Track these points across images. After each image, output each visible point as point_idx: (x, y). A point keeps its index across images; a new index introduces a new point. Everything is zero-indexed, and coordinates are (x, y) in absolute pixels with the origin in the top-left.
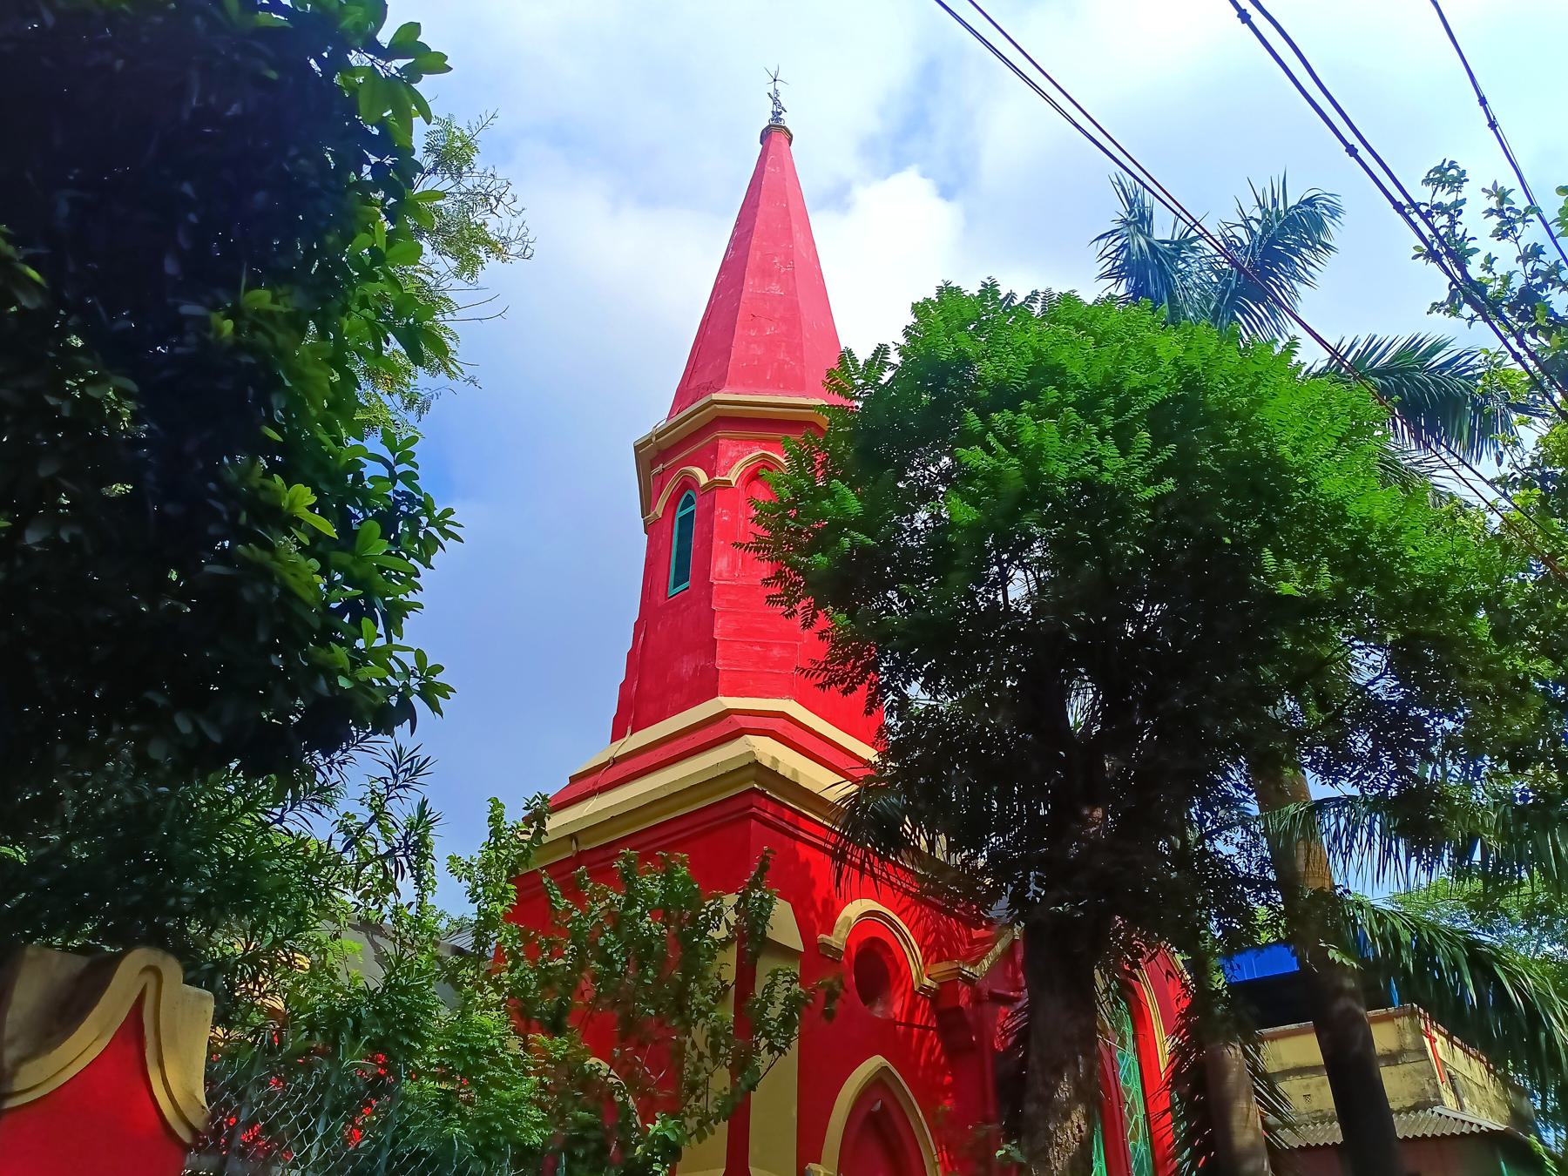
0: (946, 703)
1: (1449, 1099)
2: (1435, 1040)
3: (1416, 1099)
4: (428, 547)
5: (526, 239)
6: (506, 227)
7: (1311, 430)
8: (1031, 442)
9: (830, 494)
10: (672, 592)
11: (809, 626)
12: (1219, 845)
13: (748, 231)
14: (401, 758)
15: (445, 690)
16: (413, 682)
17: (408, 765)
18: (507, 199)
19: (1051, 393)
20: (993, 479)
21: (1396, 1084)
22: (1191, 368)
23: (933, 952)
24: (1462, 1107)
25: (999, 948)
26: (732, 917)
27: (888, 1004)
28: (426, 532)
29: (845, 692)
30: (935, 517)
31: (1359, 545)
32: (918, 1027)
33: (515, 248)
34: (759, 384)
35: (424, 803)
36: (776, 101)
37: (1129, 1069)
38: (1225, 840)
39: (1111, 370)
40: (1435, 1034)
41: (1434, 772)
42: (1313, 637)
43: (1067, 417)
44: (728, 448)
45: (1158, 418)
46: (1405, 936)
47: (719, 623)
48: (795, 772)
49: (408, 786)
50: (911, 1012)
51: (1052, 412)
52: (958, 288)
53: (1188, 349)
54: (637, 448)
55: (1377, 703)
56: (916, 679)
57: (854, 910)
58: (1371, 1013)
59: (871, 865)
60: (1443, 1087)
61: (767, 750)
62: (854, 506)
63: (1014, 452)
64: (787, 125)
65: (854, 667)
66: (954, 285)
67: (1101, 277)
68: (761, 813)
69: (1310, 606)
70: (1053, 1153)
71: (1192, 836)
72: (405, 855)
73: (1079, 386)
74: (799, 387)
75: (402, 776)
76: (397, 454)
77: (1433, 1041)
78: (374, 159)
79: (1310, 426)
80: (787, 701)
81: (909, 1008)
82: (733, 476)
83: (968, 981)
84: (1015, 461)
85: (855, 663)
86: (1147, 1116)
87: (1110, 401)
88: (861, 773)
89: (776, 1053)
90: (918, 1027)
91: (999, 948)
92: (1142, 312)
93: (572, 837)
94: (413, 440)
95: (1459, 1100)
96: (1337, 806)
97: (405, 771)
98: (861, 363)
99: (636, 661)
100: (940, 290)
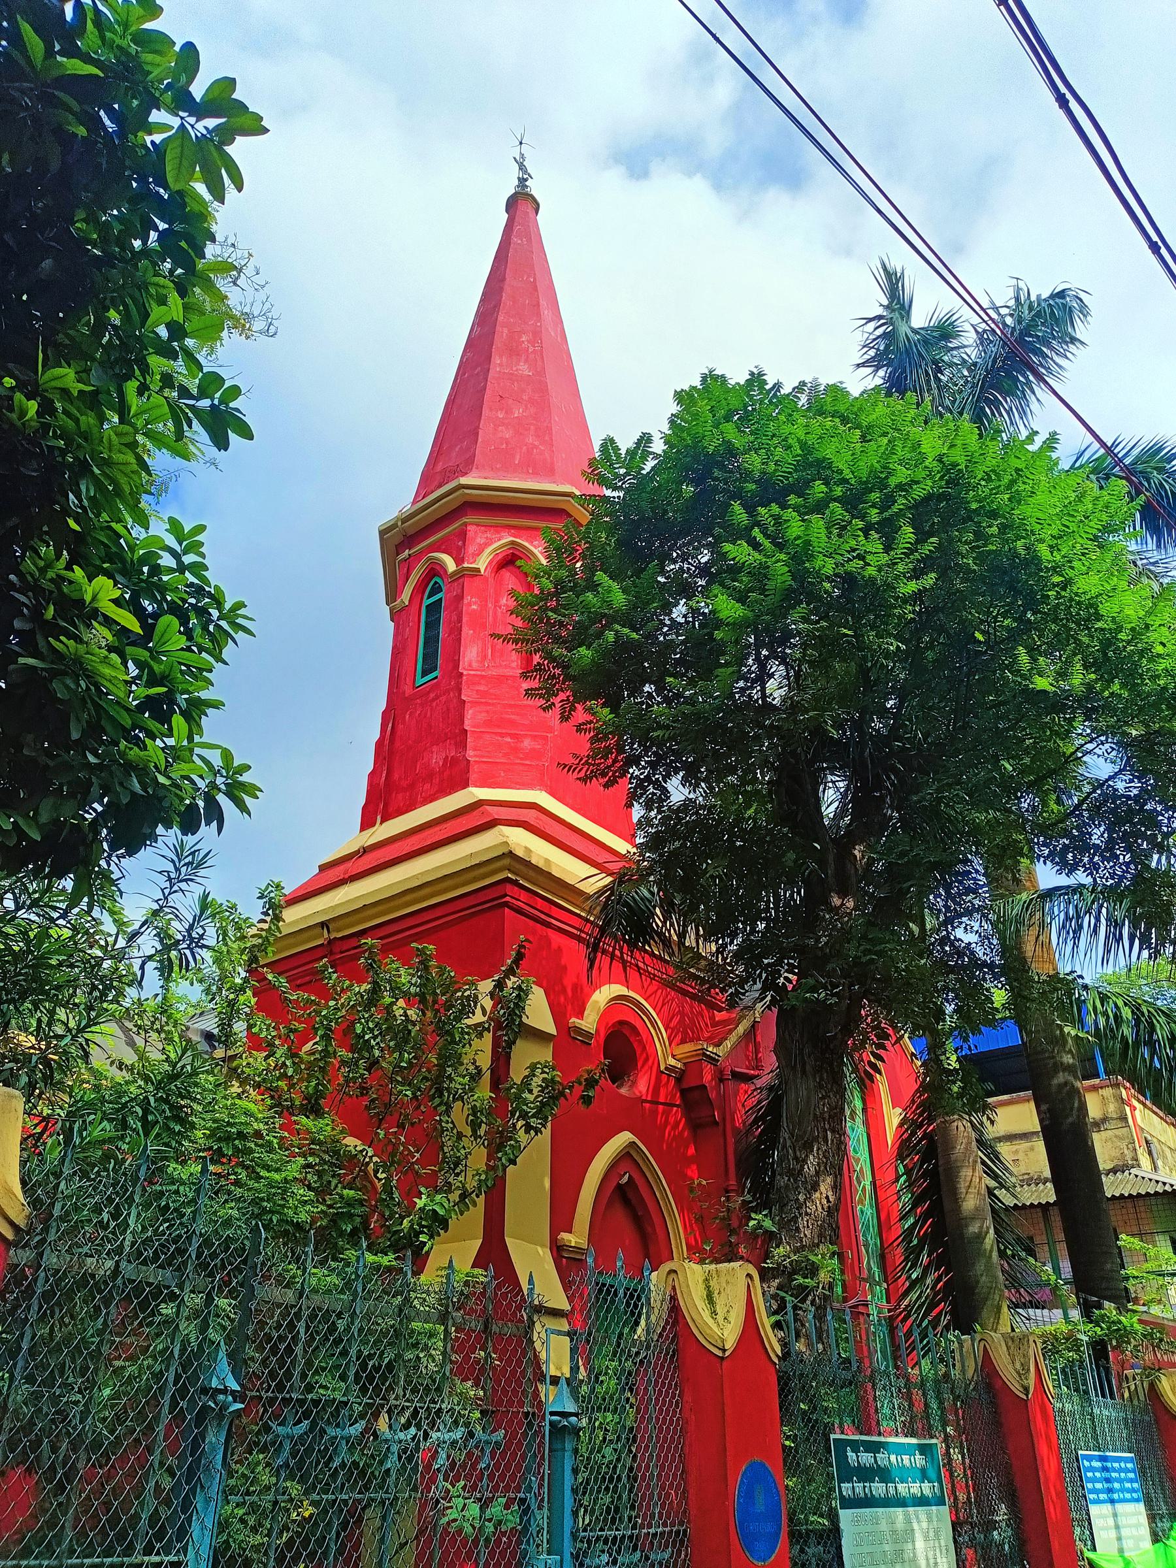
0: (698, 796)
1: (1145, 1161)
2: (1135, 1109)
3: (1116, 1162)
4: (217, 641)
5: (270, 315)
6: (249, 301)
7: (1068, 527)
8: (798, 537)
9: (593, 586)
10: (420, 681)
11: (567, 720)
12: (959, 933)
13: (495, 307)
14: (182, 851)
15: (253, 790)
16: (220, 780)
17: (190, 858)
18: (249, 271)
19: (819, 488)
20: (761, 574)
21: (1104, 1148)
22: (956, 465)
23: (680, 1033)
24: (1156, 1168)
25: (741, 1029)
26: (488, 1003)
27: (634, 1084)
28: (218, 626)
29: (606, 786)
30: (695, 612)
31: (1108, 643)
32: (662, 1104)
33: (258, 325)
34: (508, 468)
35: (206, 896)
36: (522, 167)
37: (858, 1140)
38: (965, 928)
39: (877, 465)
40: (1135, 1103)
41: (1159, 860)
42: (1057, 734)
43: (832, 513)
44: (476, 535)
45: (921, 511)
46: (1127, 1013)
47: (469, 714)
48: (547, 861)
49: (191, 880)
50: (656, 1091)
51: (820, 507)
52: (723, 376)
53: (952, 446)
54: (382, 533)
55: (1115, 795)
56: (676, 773)
57: (603, 996)
58: (1087, 1083)
59: (622, 953)
60: (1140, 1151)
61: (520, 840)
62: (619, 598)
63: (780, 547)
64: (534, 193)
65: (615, 761)
66: (718, 372)
67: (858, 366)
68: (514, 901)
69: (1055, 703)
70: (803, 1223)
71: (930, 921)
72: (188, 948)
73: (846, 481)
74: (549, 472)
75: (184, 870)
76: (185, 543)
77: (1133, 1109)
78: (162, 226)
79: (1067, 523)
80: (538, 792)
81: (654, 1087)
82: (482, 563)
83: (712, 1060)
84: (783, 557)
85: (616, 757)
86: (874, 1183)
87: (875, 496)
88: (615, 867)
89: (532, 1132)
90: (662, 1104)
91: (741, 1029)
92: (904, 407)
93: (323, 924)
94: (201, 529)
95: (1154, 1162)
96: (1067, 894)
97: (187, 864)
98: (623, 452)
99: (385, 751)
100: (704, 379)
